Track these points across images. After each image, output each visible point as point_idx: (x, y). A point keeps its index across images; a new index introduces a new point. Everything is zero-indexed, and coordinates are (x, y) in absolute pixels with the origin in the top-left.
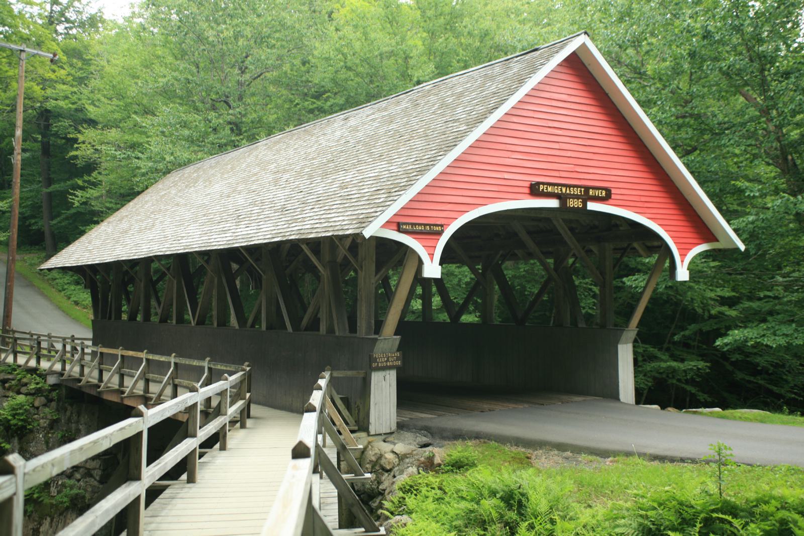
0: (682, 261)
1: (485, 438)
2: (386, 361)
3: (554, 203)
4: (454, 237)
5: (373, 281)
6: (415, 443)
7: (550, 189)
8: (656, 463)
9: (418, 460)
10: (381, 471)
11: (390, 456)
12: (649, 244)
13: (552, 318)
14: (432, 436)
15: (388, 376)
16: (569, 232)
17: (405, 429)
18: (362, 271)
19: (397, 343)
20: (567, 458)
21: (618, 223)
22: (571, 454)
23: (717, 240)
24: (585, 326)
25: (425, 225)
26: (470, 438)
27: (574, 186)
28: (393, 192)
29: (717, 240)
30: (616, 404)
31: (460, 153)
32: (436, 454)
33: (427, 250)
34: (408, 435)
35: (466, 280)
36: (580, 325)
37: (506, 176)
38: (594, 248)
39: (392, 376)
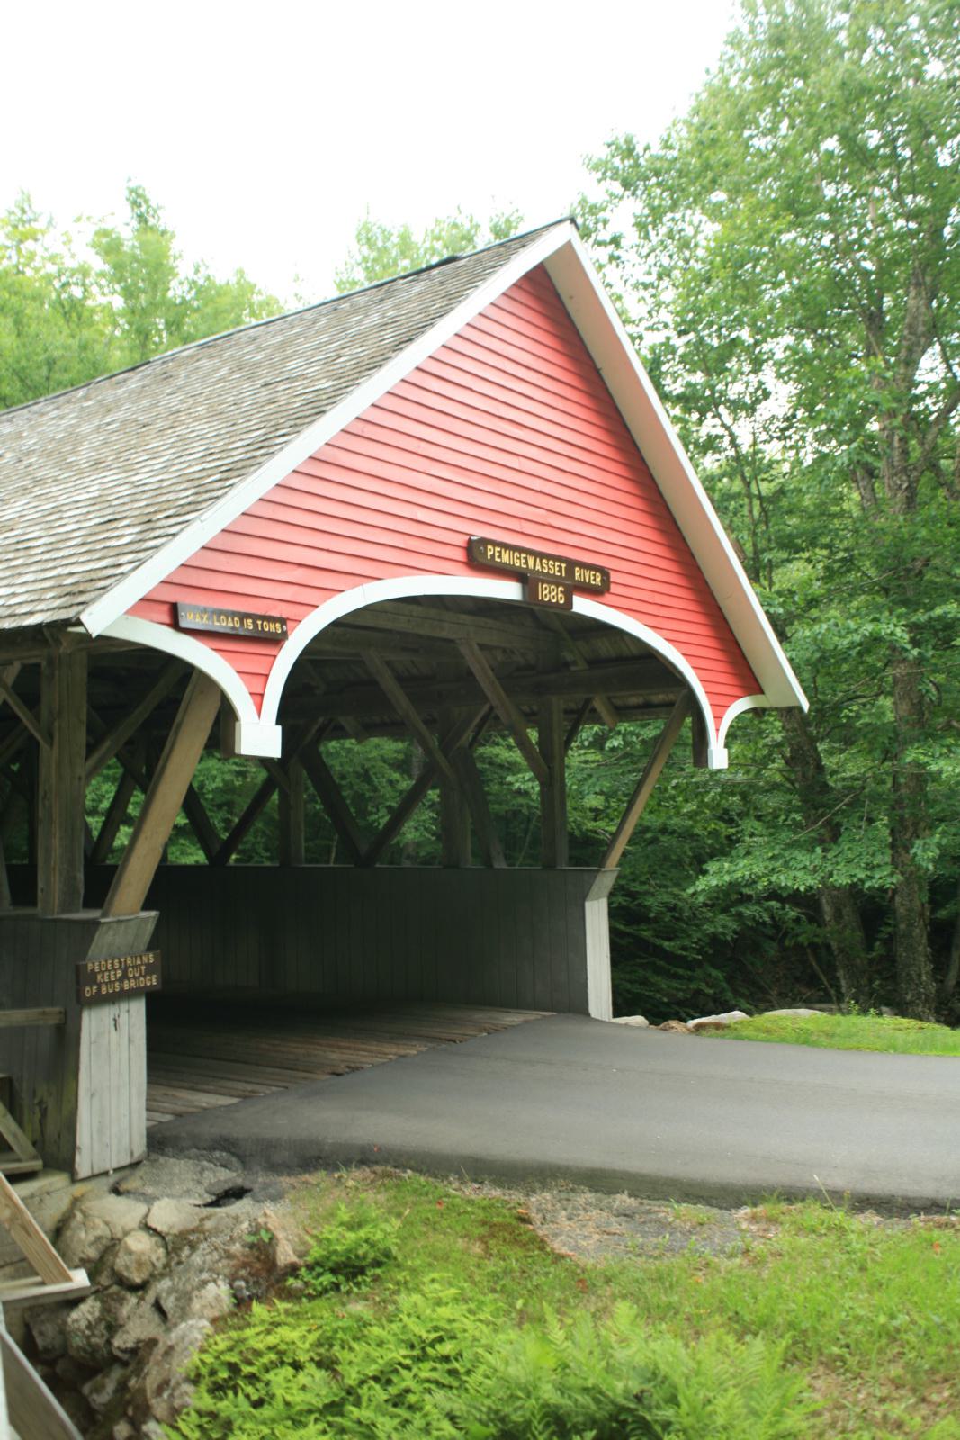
1: (386, 1162)
2: (121, 980)
3: (510, 591)
6: (201, 1189)
7: (506, 557)
8: (871, 1218)
9: (229, 1256)
10: (115, 1288)
11: (140, 1243)
13: (334, 849)
14: (243, 1162)
15: (124, 1019)
17: (169, 1150)
18: (51, 745)
19: (150, 927)
20: (628, 1215)
22: (632, 1202)
23: (761, 692)
24: (504, 866)
25: (244, 616)
26: (347, 1164)
27: (550, 557)
28: (156, 523)
29: (761, 692)
30: (571, 1026)
31: (156, 582)
32: (280, 1235)
33: (248, 684)
34: (180, 1168)
35: (214, 785)
36: (496, 865)
39: (134, 1015)
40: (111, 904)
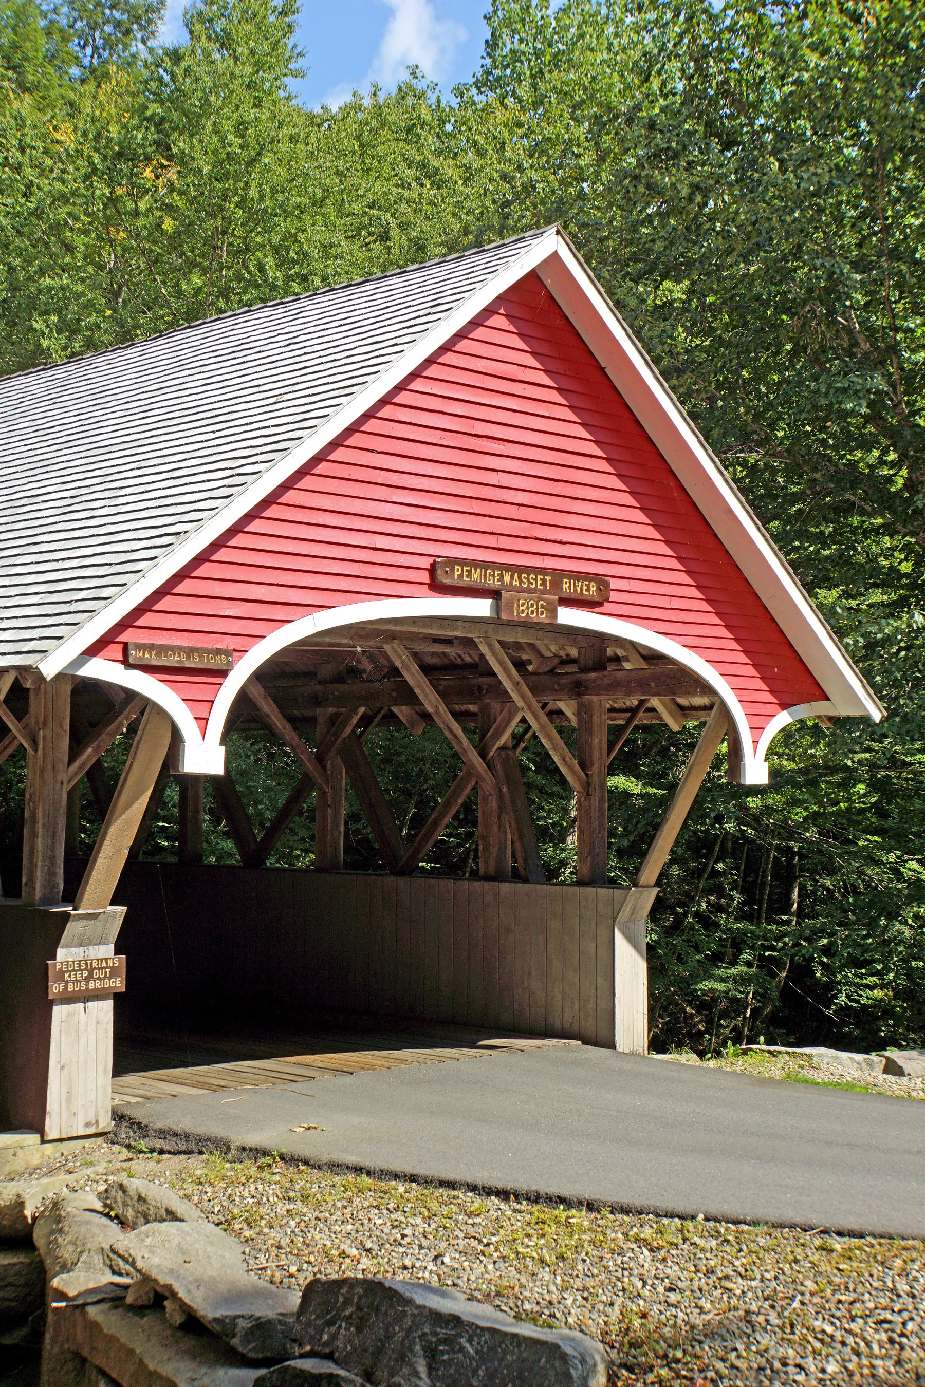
0: (756, 742)
3: (481, 608)
4: (261, 676)
5: (63, 776)
12: (683, 701)
16: (514, 671)
19: (118, 923)
21: (620, 653)
37: (380, 542)
38: (568, 707)
39: (103, 1012)
40: (81, 900)
